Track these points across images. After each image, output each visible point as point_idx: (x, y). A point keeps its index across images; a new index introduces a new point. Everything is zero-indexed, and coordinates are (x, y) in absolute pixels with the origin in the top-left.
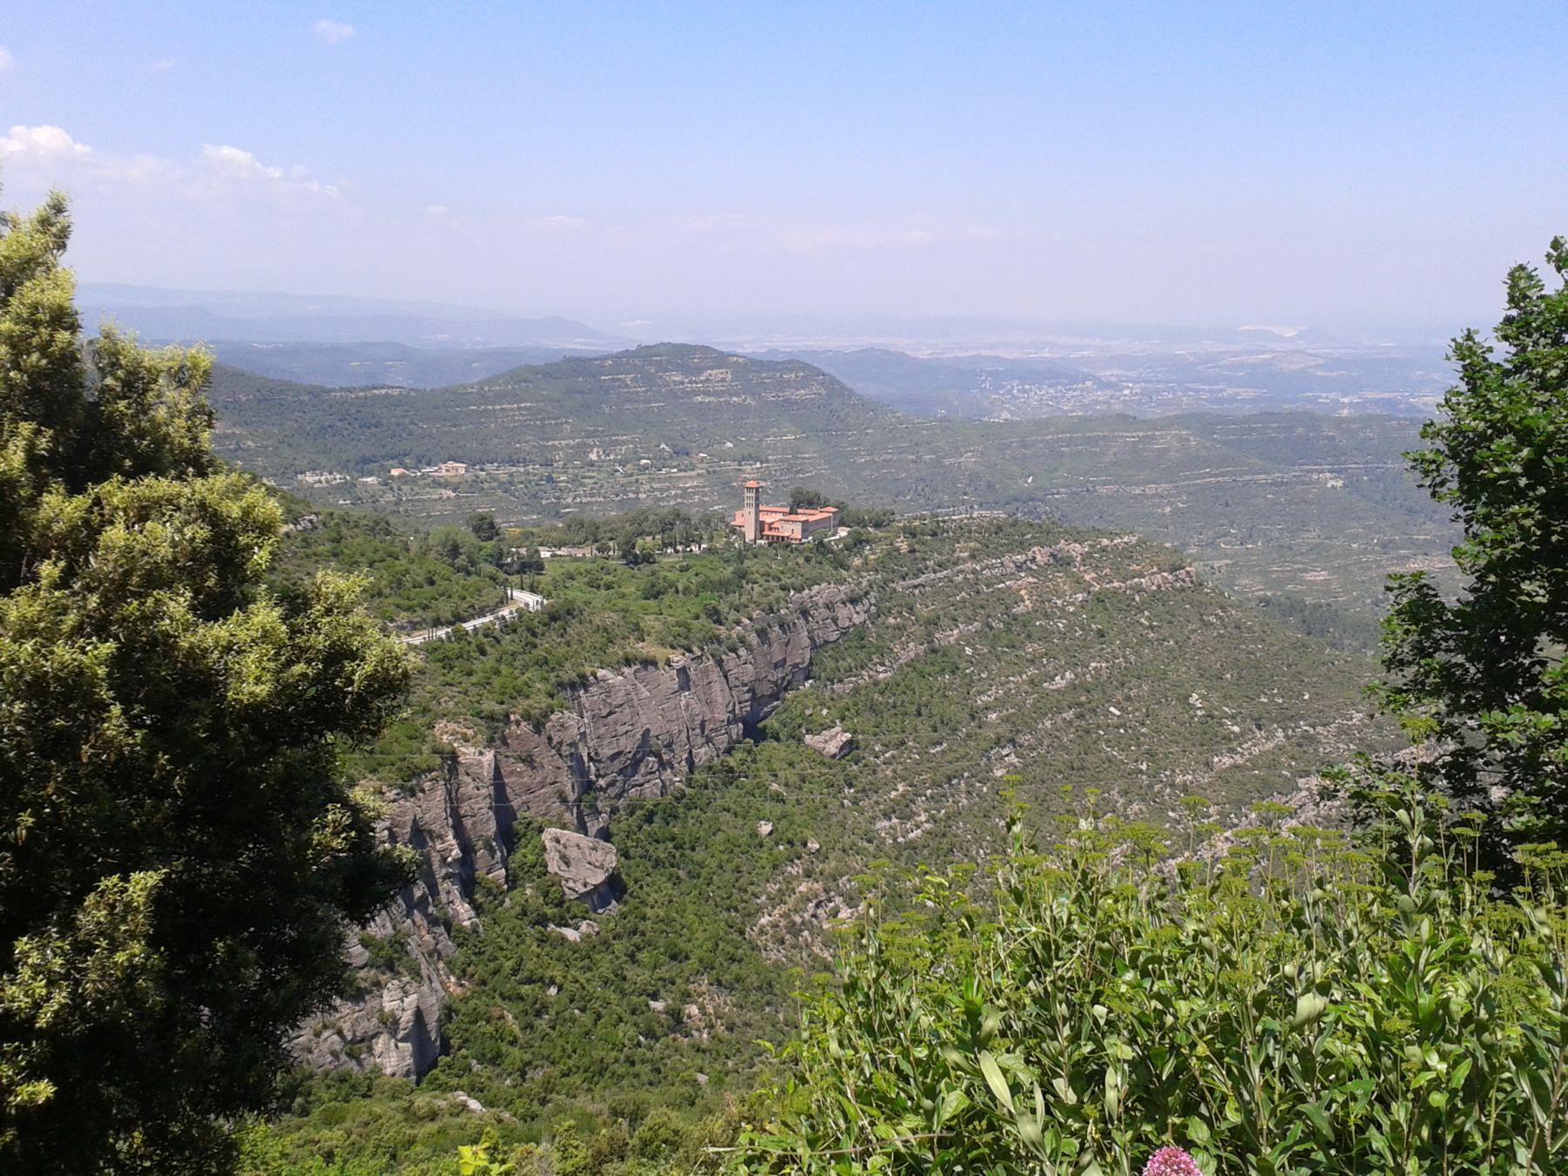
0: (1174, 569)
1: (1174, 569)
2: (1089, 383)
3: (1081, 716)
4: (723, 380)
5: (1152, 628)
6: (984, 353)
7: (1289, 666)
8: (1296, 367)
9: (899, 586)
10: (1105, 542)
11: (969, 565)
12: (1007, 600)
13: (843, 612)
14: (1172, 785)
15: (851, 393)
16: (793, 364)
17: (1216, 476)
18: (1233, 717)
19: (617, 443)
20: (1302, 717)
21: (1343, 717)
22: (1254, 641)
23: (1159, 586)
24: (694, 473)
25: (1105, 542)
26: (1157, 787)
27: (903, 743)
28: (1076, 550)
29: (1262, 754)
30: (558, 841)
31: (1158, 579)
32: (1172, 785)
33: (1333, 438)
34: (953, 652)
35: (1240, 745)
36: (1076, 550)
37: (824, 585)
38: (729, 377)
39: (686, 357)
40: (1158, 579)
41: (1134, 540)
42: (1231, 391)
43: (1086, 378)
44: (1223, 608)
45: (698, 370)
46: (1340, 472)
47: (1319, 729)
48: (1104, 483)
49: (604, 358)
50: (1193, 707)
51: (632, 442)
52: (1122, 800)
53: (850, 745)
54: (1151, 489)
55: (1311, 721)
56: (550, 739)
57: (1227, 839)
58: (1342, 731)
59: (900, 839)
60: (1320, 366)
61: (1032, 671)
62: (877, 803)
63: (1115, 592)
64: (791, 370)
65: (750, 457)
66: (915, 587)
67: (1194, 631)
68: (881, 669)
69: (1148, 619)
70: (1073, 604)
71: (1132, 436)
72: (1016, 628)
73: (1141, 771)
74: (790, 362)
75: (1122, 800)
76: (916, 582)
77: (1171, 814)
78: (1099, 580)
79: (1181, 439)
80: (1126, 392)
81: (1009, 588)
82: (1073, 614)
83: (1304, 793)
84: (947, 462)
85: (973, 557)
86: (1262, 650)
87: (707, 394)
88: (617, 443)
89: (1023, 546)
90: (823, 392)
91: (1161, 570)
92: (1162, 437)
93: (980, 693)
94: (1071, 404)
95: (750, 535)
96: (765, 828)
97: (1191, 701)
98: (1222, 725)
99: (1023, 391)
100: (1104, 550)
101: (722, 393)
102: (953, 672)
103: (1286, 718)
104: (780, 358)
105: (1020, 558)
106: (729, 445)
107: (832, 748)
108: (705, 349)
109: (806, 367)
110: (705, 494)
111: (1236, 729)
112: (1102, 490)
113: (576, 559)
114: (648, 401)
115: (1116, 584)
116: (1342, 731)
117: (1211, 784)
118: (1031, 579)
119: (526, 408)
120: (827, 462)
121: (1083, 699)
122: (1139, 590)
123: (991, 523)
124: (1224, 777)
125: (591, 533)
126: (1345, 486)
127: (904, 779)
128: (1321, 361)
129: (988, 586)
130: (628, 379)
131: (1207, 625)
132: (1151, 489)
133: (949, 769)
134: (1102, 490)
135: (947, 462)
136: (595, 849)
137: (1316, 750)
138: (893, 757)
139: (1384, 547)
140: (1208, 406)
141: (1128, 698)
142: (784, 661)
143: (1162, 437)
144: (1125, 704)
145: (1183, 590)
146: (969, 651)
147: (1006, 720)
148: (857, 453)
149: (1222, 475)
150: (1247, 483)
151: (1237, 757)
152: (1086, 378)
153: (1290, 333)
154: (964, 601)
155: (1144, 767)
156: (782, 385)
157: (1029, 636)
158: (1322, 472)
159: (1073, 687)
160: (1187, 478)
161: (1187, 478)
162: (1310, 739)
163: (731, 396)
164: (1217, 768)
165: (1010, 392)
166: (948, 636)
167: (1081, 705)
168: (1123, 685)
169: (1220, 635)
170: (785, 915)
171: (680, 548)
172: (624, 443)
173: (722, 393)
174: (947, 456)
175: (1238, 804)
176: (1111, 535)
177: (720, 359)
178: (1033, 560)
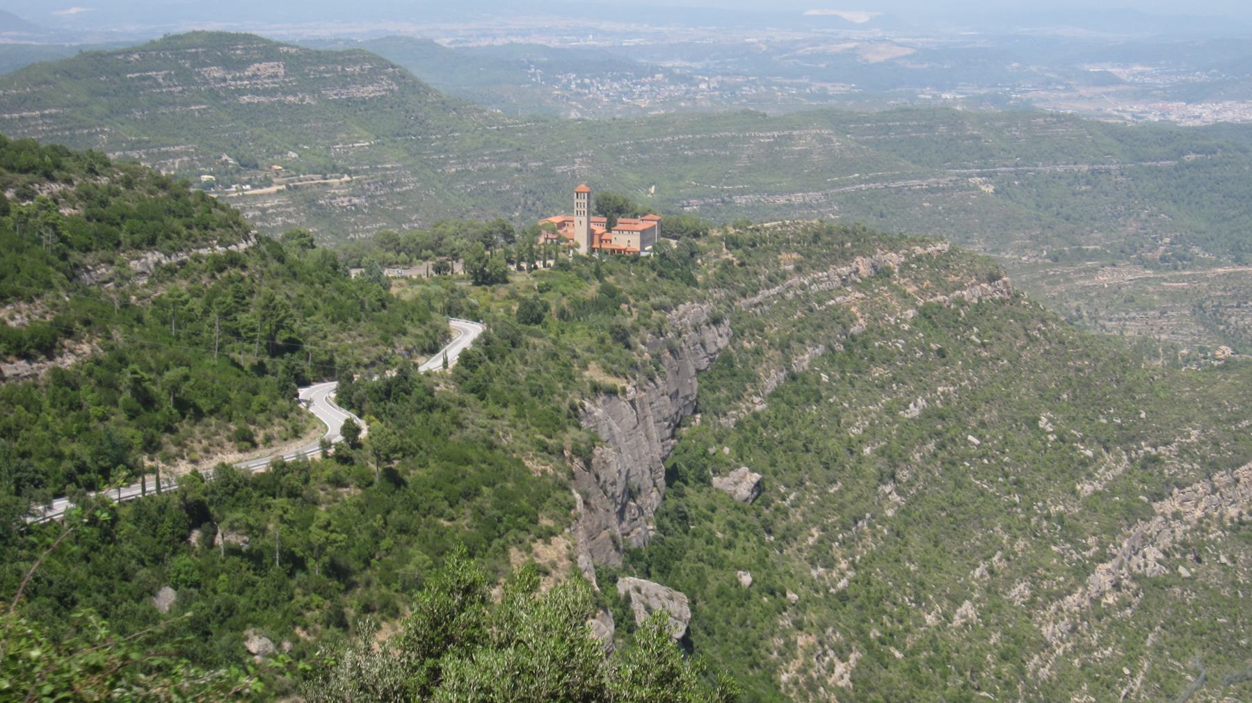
0: (992, 278)
1: (992, 278)
2: (659, 76)
3: (942, 446)
4: (275, 76)
5: (984, 345)
6: (519, 40)
7: (1118, 382)
8: (881, 59)
9: (742, 303)
10: (919, 250)
11: (795, 280)
12: (840, 318)
13: (710, 334)
14: (1048, 517)
15: (428, 90)
16: (352, 56)
17: (866, 181)
18: (1082, 441)
19: (167, 155)
20: (1143, 438)
21: (1181, 433)
22: (1080, 357)
23: (980, 299)
24: (274, 189)
25: (919, 250)
26: (1034, 520)
27: (802, 483)
28: (893, 259)
29: (1116, 479)
30: (639, 590)
31: (977, 291)
32: (1048, 517)
33: (978, 138)
34: (811, 379)
35: (1096, 470)
36: (893, 259)
37: (688, 303)
38: (282, 71)
39: (227, 49)
40: (977, 291)
41: (946, 247)
42: (816, 87)
43: (653, 71)
44: (1043, 321)
45: (242, 64)
46: (990, 176)
47: (1161, 449)
48: (742, 193)
49: (129, 52)
50: (1044, 432)
51: (187, 153)
52: (1006, 537)
53: (759, 487)
54: (797, 198)
55: (1152, 440)
56: (598, 477)
57: (1108, 571)
58: (1184, 451)
59: (832, 590)
60: (908, 57)
61: (885, 400)
62: (800, 550)
63: (940, 306)
64: (355, 62)
65: (335, 169)
66: (756, 306)
67: (1023, 348)
68: (757, 400)
69: (978, 336)
70: (905, 321)
71: (766, 137)
72: (858, 351)
73: (1015, 505)
74: (351, 52)
75: (1006, 537)
76: (756, 300)
77: (1054, 548)
78: (922, 292)
79: (825, 140)
80: (703, 86)
81: (839, 305)
82: (910, 332)
83: (1160, 519)
84: (558, 170)
85: (798, 269)
86: (1089, 366)
87: (256, 92)
88: (167, 155)
89: (846, 257)
90: (396, 88)
91: (980, 281)
92: (800, 137)
93: (849, 424)
94: (645, 101)
95: (583, 250)
96: (746, 579)
97: (1041, 424)
98: (1074, 449)
99: (584, 86)
100: (919, 259)
101: (272, 92)
102: (817, 401)
103: (1128, 438)
104: (340, 47)
105: (845, 270)
106: (293, 155)
107: (744, 491)
108: (248, 38)
109: (371, 58)
110: (290, 216)
111: (1089, 453)
112: (740, 200)
113: (412, 282)
114: (187, 104)
115: (940, 298)
116: (1184, 451)
117: (1082, 514)
118: (858, 295)
119: (51, 116)
120: (415, 173)
121: (939, 427)
122: (961, 302)
123: (805, 230)
124: (1091, 505)
125: (433, 248)
126: (996, 192)
127: (815, 523)
128: (909, 51)
129: (820, 303)
130: (160, 76)
131: (1032, 340)
132: (797, 198)
133: (851, 510)
134: (740, 200)
135: (558, 170)
136: (671, 598)
137: (1161, 473)
138: (798, 498)
139: (1056, 260)
140: (806, 102)
141: (983, 424)
142: (677, 392)
143: (800, 137)
144: (981, 431)
145: (1003, 301)
146: (825, 378)
147: (882, 452)
148: (445, 162)
149: (874, 180)
150: (899, 190)
151: (1096, 484)
152: (653, 71)
153: (862, 18)
154: (801, 320)
155: (1017, 499)
156: (345, 81)
157: (872, 359)
158: (971, 176)
159: (926, 415)
160: (834, 185)
161: (834, 185)
162: (1155, 460)
163: (285, 94)
164: (1083, 494)
165: (566, 87)
166: (803, 360)
167: (939, 434)
168: (974, 409)
169: (1047, 352)
170: (802, 671)
171: (524, 265)
172: (177, 155)
173: (272, 92)
174: (558, 163)
175: (1113, 531)
176: (923, 242)
177: (269, 50)
178: (857, 271)
